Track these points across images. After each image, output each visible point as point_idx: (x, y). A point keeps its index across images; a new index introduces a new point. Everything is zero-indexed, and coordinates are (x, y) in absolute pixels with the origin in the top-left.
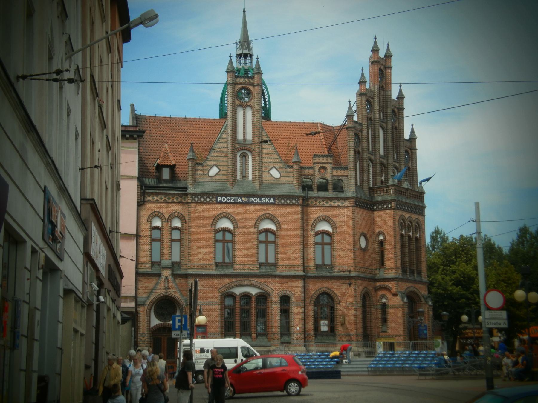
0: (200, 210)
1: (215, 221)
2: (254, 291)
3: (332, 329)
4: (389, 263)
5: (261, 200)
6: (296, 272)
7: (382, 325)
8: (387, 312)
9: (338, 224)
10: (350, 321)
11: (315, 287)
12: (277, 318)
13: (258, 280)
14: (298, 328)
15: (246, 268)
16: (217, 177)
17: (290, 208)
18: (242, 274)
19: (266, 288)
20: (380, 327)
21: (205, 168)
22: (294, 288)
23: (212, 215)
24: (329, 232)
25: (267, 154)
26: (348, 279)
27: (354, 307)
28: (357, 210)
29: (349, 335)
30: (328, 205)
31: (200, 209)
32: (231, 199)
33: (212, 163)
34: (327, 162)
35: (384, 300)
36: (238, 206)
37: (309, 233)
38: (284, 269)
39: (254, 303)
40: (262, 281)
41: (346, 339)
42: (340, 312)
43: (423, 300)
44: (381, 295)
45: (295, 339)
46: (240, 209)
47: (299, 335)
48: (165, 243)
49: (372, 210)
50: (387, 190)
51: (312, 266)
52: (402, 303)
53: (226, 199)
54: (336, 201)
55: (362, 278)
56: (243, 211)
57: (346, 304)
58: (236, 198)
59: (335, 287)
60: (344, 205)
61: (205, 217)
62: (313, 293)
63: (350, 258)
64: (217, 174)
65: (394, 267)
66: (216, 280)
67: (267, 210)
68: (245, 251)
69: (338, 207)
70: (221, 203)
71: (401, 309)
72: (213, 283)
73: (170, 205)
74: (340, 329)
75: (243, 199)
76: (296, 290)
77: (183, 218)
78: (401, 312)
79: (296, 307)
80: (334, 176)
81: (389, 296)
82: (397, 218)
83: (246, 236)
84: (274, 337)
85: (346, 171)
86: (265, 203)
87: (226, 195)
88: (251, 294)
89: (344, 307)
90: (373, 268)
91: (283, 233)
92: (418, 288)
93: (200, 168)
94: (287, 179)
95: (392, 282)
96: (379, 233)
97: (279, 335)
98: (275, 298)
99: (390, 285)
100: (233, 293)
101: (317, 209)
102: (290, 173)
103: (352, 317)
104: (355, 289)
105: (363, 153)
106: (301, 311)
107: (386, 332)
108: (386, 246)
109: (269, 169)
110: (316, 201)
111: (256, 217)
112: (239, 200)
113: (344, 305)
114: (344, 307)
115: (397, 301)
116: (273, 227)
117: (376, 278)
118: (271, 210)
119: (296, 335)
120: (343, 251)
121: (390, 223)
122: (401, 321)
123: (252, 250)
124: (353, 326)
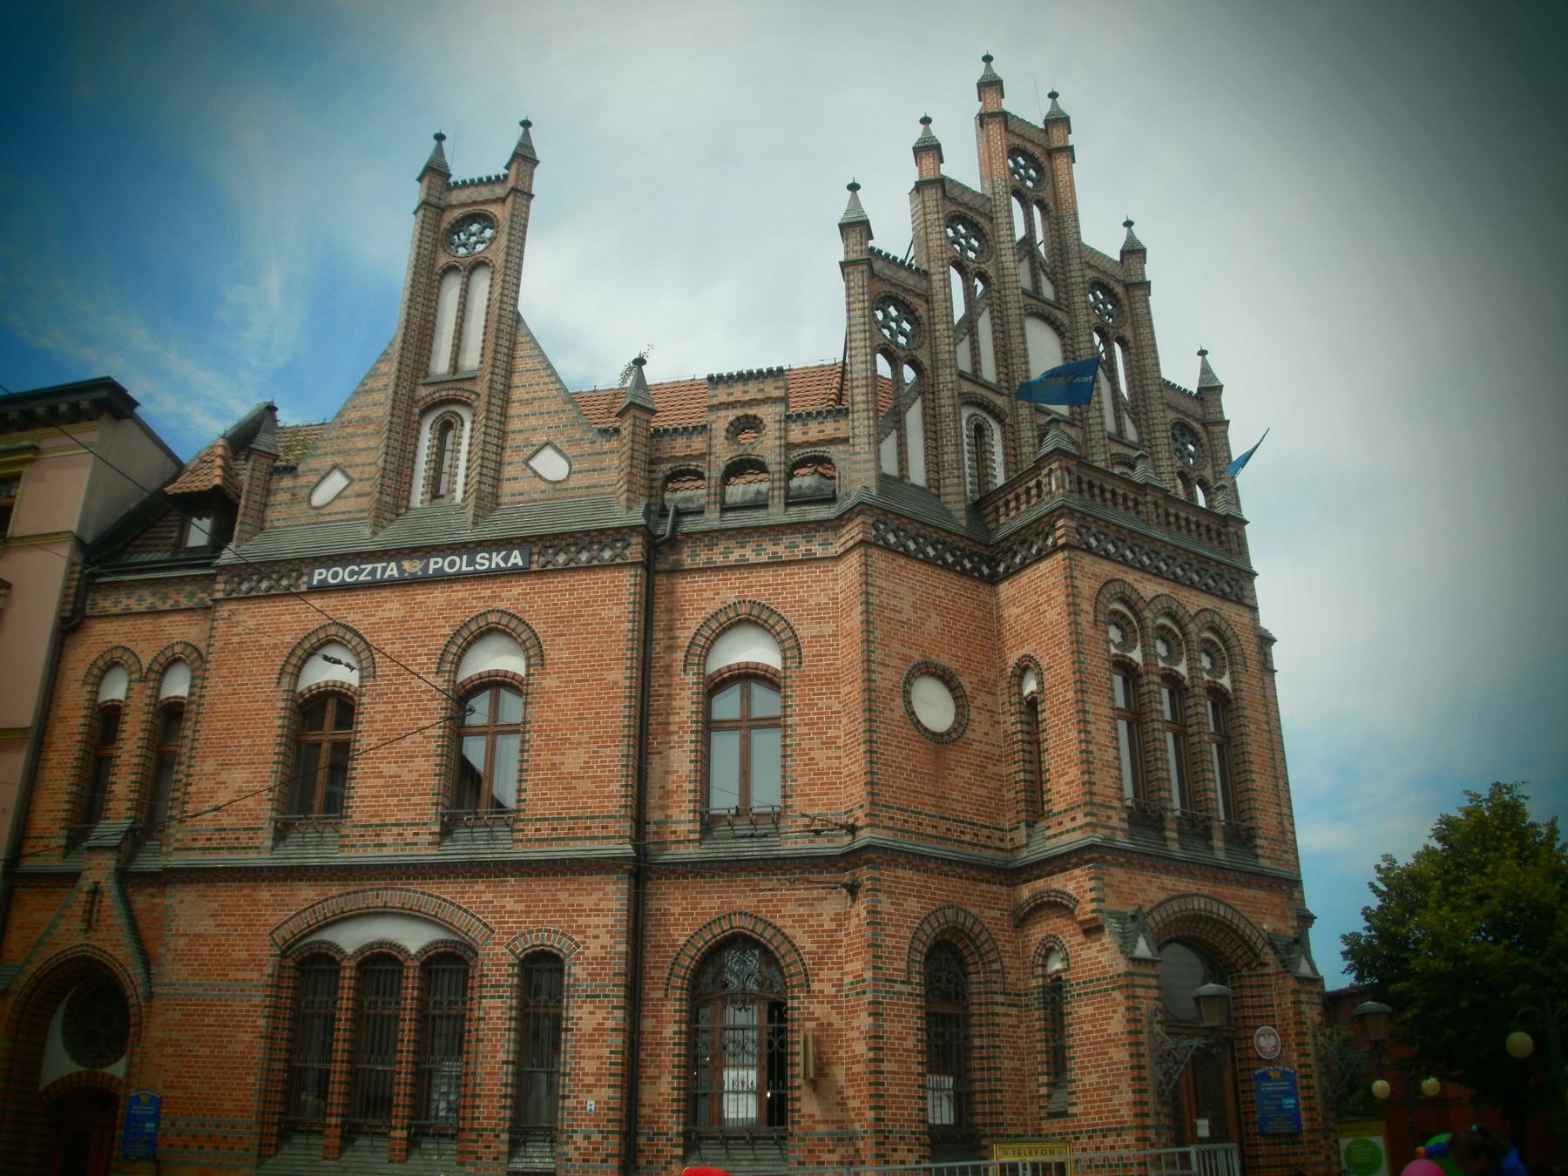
0: (251, 623)
2: (414, 939)
3: (776, 1111)
4: (1063, 785)
5: (471, 562)
6: (595, 845)
7: (1051, 1085)
8: (1068, 1020)
9: (805, 631)
10: (857, 1068)
11: (688, 917)
12: (502, 1056)
13: (432, 887)
14: (591, 1105)
15: (387, 839)
16: (340, 506)
17: (587, 579)
18: (372, 861)
19: (461, 921)
20: (1043, 1090)
21: (303, 481)
22: (582, 921)
23: (288, 639)
24: (767, 668)
25: (526, 403)
26: (844, 867)
27: (869, 997)
28: (879, 559)
29: (852, 1138)
30: (764, 558)
31: (249, 618)
32: (359, 573)
33: (328, 462)
34: (760, 396)
35: (1055, 965)
36: (386, 593)
37: (677, 680)
38: (545, 833)
39: (410, 991)
40: (448, 890)
41: (835, 1157)
42: (811, 1025)
43: (1269, 957)
44: (1043, 944)
45: (574, 1155)
46: (392, 606)
47: (596, 1137)
48: (125, 757)
49: (993, 580)
50: (1039, 485)
51: (681, 818)
52: (1121, 966)
53: (344, 575)
54: (798, 539)
55: (917, 861)
56: (402, 613)
57: (839, 985)
58: (380, 566)
59: (789, 908)
60: (832, 551)
61: (260, 648)
62: (682, 941)
63: (855, 768)
64: (338, 496)
65: (1081, 800)
66: (265, 894)
67: (494, 597)
68: (394, 770)
69: (809, 560)
70: (323, 589)
71: (1118, 995)
72: (255, 902)
73: (165, 621)
74: (806, 1106)
75: (406, 565)
76: (592, 925)
78: (1121, 1010)
79: (588, 1007)
80: (790, 446)
81: (1072, 939)
82: (1087, 587)
83: (402, 707)
84: (479, 1147)
85: (843, 424)
86: (489, 570)
87: (343, 559)
88: (402, 950)
89: (830, 999)
90: (1007, 826)
91: (550, 682)
92: (1237, 904)
93: (287, 482)
94: (594, 478)
95: (1077, 872)
96: (1022, 669)
97: (505, 1137)
98: (497, 965)
99: (1070, 888)
100: (331, 945)
101: (714, 578)
102: (608, 457)
103: (861, 1048)
104: (872, 912)
105: (935, 368)
106: (610, 1024)
107: (1063, 1114)
108: (203, 731)
109: (527, 452)
110: (710, 547)
111: (448, 631)
112: (392, 570)
113: (829, 990)
114: (830, 999)
115: (1104, 958)
116: (511, 662)
117: (1018, 864)
118: (510, 596)
119: (578, 1138)
120: (829, 743)
121: (1055, 613)
122: (1121, 1055)
123: (420, 763)
124: (866, 1091)
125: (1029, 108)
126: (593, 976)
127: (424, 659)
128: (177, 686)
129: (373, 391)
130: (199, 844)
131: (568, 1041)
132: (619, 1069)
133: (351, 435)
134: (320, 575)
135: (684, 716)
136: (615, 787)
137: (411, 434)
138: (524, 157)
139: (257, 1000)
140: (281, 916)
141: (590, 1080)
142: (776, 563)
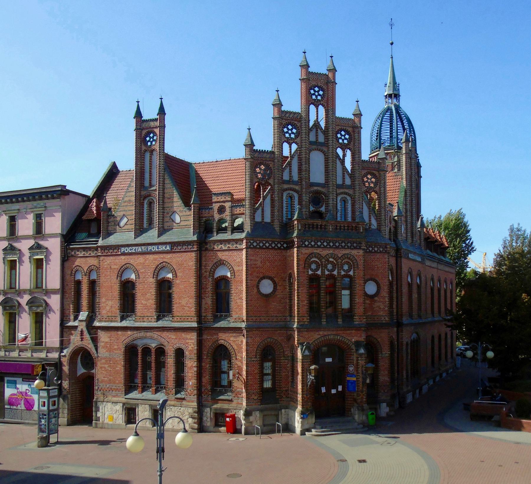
1: (232, 271)
12: (172, 372)
14: (191, 383)
22: (187, 341)
30: (226, 248)
32: (132, 250)
46: (141, 259)
48: (84, 296)
58: (137, 248)
66: (120, 333)
67: (164, 258)
68: (145, 303)
70: (124, 254)
75: (143, 247)
77: (213, 270)
83: (146, 286)
91: (178, 282)
106: (194, 365)
109: (170, 214)
112: (140, 250)
119: (188, 390)
125: (319, 67)
126: (190, 354)
127: (149, 274)
128: (94, 276)
129: (130, 192)
130: (104, 320)
131: (186, 369)
132: (196, 376)
133: (127, 206)
134: (123, 249)
135: (209, 289)
136: (193, 309)
137: (142, 205)
138: (162, 111)
139: (121, 358)
140: (124, 338)
141: (190, 378)
142: (229, 250)
